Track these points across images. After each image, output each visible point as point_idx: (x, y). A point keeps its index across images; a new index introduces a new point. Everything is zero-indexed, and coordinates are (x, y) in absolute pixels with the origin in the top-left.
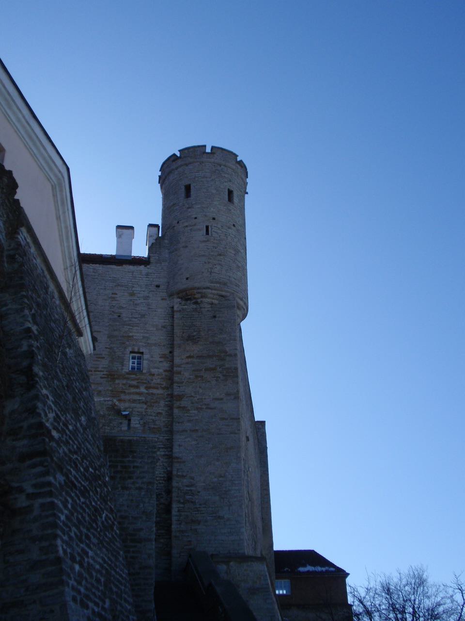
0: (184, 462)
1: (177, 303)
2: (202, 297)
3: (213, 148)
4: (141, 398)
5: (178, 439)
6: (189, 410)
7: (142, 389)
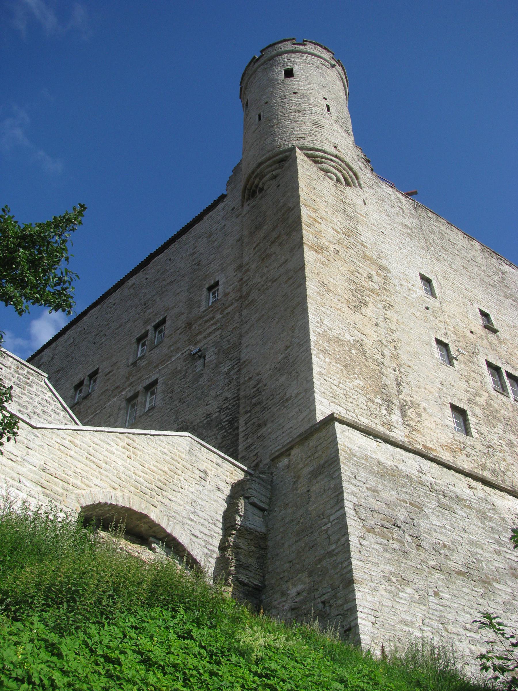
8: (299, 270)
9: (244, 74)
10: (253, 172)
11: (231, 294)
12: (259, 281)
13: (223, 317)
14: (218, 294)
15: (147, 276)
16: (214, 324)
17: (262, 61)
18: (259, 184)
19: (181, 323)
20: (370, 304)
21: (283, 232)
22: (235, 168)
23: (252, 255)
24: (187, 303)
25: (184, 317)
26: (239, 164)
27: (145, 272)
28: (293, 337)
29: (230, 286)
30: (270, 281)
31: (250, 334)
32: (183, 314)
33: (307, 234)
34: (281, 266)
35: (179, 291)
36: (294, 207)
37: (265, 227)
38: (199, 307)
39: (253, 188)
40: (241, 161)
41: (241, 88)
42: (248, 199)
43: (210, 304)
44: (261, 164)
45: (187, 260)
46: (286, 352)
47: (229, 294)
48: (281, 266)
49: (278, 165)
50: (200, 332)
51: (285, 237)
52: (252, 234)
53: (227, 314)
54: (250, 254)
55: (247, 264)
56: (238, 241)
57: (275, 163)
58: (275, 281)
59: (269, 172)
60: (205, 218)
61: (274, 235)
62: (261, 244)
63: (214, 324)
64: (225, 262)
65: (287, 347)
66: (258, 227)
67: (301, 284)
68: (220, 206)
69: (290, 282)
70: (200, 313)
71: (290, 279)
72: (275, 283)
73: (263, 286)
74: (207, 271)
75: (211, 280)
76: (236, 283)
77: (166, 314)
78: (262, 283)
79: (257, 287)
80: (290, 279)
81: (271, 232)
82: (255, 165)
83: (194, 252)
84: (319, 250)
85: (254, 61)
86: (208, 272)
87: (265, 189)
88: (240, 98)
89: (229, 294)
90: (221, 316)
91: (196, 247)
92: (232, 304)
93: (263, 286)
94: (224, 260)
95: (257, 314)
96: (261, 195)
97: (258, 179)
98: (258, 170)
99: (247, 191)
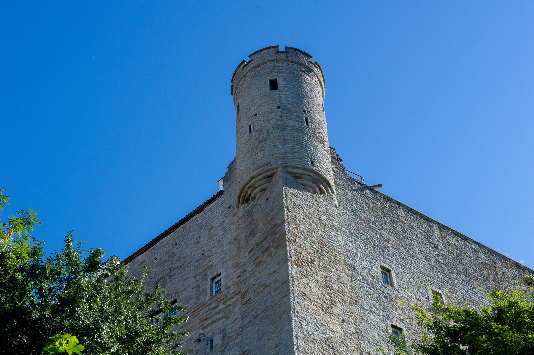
2: (253, 190)
8: (285, 282)
9: (234, 74)
10: (247, 184)
11: (232, 288)
12: (254, 283)
13: (225, 307)
14: (220, 284)
15: (156, 256)
16: (218, 312)
17: (251, 66)
18: (251, 193)
19: (190, 306)
20: (338, 304)
21: (272, 245)
22: (230, 165)
23: (248, 258)
24: (195, 289)
25: (192, 301)
26: (233, 162)
27: (153, 251)
28: (281, 338)
29: (230, 280)
30: (263, 286)
31: (248, 328)
32: (191, 299)
33: (292, 250)
34: (271, 274)
35: (186, 276)
36: (280, 225)
37: (258, 235)
38: (206, 295)
39: (247, 196)
40: (235, 159)
41: (232, 86)
42: (243, 203)
43: (214, 294)
44: (253, 178)
45: (192, 248)
46: (276, 350)
47: (229, 287)
48: (271, 274)
49: (266, 179)
50: (207, 318)
51: (273, 249)
52: (247, 238)
53: (229, 305)
54: (246, 257)
55: (244, 265)
56: (235, 239)
57: (264, 178)
58: (267, 287)
59: (260, 186)
60: (206, 209)
61: (265, 245)
62: (255, 250)
63: (218, 312)
64: (225, 257)
65: (277, 346)
66: (252, 233)
67: (286, 296)
68: (218, 201)
69: (278, 291)
70: (206, 301)
71: (278, 288)
72: (266, 289)
73: (257, 288)
74: (210, 262)
75: (214, 271)
76: (235, 279)
77: (176, 297)
78: (256, 286)
79: (253, 288)
80: (278, 288)
81: (262, 241)
82: (248, 178)
83: (198, 241)
84: (299, 262)
85: (243, 64)
86: (211, 263)
87: (256, 198)
88: (232, 94)
89: (229, 287)
90: (224, 306)
91: (199, 237)
92: (232, 298)
93: (257, 288)
94: (224, 255)
95: (253, 312)
96: (253, 202)
97: (250, 189)
98: (251, 183)
99: (241, 197)
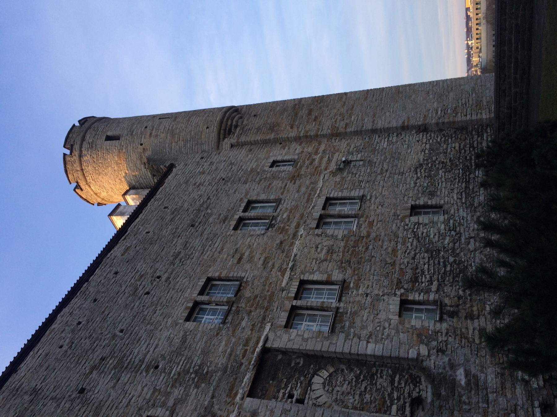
0: (409, 118)
1: (227, 143)
2: (232, 120)
3: (79, 121)
4: (327, 157)
5: (380, 124)
6: (351, 121)
7: (317, 157)
